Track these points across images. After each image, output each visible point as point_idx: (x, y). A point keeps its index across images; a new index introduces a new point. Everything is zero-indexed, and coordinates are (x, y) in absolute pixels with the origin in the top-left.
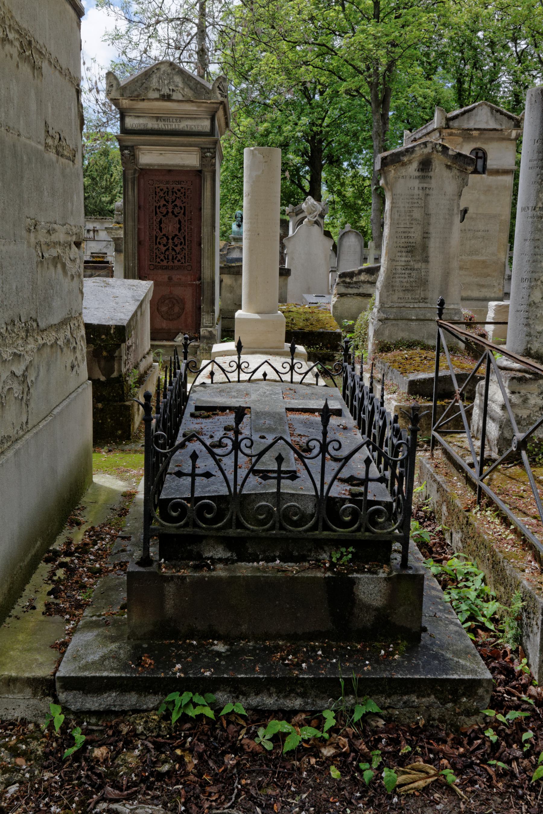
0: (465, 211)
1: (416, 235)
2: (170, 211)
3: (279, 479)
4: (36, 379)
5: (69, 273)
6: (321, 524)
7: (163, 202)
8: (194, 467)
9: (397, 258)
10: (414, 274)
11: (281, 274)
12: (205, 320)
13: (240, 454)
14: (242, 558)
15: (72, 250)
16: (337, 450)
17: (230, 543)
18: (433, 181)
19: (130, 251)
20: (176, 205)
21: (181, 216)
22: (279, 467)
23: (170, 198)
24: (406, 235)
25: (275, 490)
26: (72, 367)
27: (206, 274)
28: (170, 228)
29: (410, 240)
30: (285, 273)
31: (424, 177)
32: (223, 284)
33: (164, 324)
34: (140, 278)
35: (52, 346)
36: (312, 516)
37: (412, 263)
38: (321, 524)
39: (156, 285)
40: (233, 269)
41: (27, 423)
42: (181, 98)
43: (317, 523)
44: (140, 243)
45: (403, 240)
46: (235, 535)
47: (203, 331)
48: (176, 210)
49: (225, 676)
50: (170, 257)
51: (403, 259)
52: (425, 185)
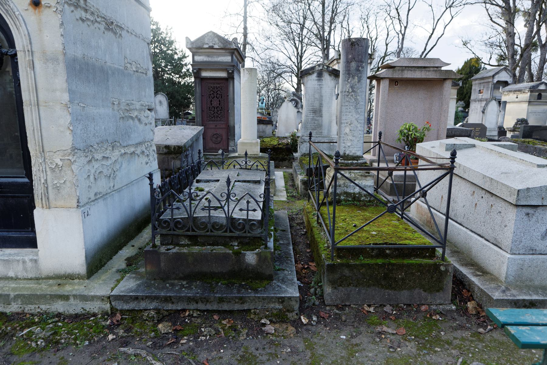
1: (317, 105)
3: (209, 210)
5: (144, 123)
6: (228, 230)
7: (212, 92)
10: (316, 122)
17: (190, 237)
18: (324, 81)
22: (209, 205)
23: (215, 90)
28: (215, 103)
31: (319, 80)
33: (214, 146)
35: (131, 154)
36: (225, 226)
38: (228, 230)
41: (114, 186)
42: (218, 47)
43: (227, 229)
44: (202, 111)
47: (230, 148)
48: (218, 96)
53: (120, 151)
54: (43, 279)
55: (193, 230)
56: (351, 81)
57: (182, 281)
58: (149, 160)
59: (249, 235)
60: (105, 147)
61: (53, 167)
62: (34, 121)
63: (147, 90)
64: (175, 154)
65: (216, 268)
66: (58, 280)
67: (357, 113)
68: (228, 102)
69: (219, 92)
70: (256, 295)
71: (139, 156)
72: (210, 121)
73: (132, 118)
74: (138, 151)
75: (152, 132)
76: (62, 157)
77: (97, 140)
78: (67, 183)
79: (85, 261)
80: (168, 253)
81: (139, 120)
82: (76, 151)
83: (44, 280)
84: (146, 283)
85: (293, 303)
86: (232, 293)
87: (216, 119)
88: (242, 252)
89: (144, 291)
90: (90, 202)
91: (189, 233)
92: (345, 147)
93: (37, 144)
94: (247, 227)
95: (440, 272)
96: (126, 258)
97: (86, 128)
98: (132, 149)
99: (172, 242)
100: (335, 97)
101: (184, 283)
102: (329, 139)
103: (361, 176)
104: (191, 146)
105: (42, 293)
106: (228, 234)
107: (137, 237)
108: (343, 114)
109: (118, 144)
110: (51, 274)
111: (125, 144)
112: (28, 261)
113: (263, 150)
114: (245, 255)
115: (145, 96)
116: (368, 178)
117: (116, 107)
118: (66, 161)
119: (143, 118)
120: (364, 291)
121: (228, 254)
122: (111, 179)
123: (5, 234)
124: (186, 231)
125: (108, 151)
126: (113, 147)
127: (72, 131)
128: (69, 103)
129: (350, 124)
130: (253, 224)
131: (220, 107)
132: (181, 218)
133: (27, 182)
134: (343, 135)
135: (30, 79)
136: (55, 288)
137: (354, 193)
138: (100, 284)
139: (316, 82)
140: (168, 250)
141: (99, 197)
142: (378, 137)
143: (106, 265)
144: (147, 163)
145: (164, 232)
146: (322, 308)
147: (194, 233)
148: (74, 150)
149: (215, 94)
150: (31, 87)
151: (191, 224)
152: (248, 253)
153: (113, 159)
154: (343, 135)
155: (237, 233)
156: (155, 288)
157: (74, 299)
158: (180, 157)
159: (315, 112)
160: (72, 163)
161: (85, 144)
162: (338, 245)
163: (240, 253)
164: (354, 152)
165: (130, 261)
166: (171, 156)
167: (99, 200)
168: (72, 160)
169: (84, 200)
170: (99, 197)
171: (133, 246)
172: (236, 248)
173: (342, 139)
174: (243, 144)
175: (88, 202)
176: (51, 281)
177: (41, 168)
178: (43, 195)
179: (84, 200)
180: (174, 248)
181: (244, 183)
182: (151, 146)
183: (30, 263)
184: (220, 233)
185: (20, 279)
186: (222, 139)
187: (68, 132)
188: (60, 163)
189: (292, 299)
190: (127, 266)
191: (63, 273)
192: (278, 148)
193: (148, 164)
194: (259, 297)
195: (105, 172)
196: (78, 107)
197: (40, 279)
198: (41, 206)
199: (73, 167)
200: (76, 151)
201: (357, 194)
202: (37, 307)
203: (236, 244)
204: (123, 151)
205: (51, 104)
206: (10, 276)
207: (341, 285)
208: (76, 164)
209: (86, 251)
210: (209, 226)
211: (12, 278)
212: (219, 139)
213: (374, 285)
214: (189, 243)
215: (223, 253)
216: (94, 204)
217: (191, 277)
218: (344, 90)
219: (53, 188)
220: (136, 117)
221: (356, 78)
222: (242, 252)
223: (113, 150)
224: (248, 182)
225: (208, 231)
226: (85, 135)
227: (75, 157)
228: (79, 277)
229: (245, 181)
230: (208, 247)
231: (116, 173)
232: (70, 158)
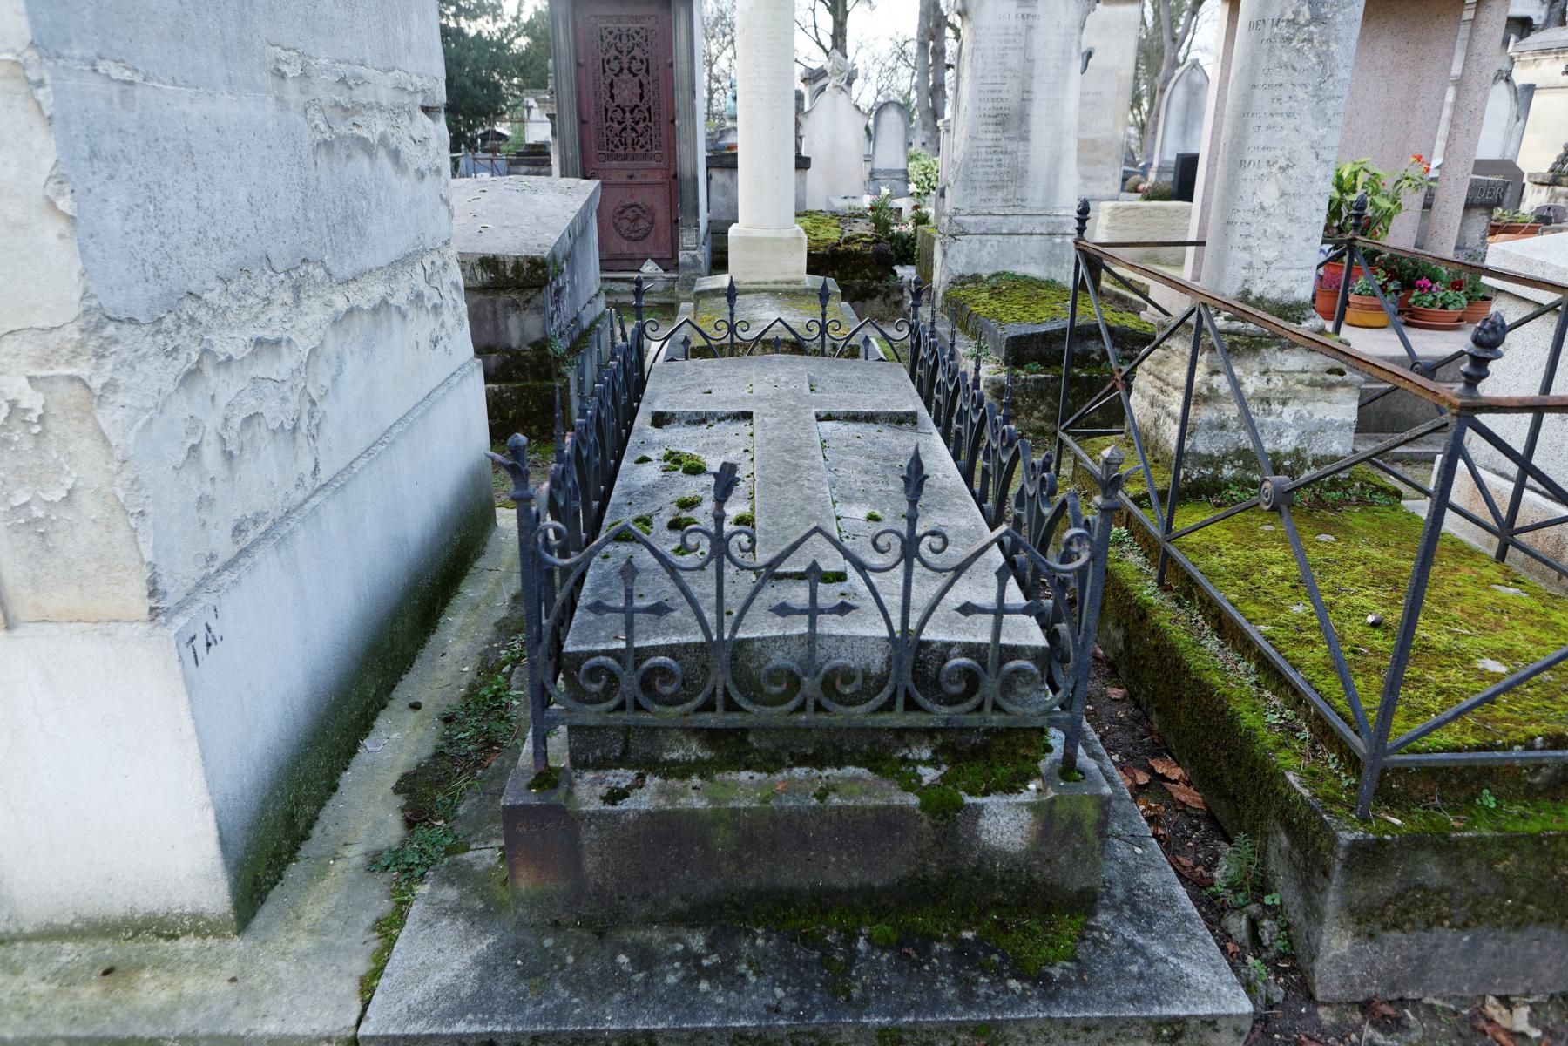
0: (1089, 55)
2: (625, 65)
4: (334, 380)
5: (412, 168)
6: (900, 700)
7: (613, 52)
8: (629, 597)
9: (981, 135)
10: (1006, 160)
11: (798, 167)
12: (686, 239)
13: (730, 571)
14: (739, 760)
15: (417, 122)
16: (937, 552)
17: (711, 736)
19: (568, 133)
20: (634, 58)
21: (642, 74)
23: (625, 44)
24: (995, 95)
25: (806, 630)
26: (435, 342)
27: (684, 167)
29: (1002, 104)
30: (802, 163)
32: (713, 183)
33: (625, 247)
34: (585, 177)
35: (375, 310)
37: (1003, 142)
39: (603, 185)
40: (724, 160)
41: (316, 469)
44: (582, 122)
45: (991, 105)
46: (721, 725)
48: (635, 65)
49: (709, 1025)
50: (629, 142)
51: (990, 136)
52: (1027, 11)
53: (328, 304)
54: (29, 938)
55: (731, 706)
57: (683, 932)
58: (442, 326)
59: (996, 720)
60: (261, 291)
63: (415, 18)
64: (520, 288)
65: (842, 871)
66: (101, 943)
67: (1322, 117)
68: (671, 91)
69: (637, 52)
70: (1057, 1014)
71: (404, 316)
72: (608, 158)
73: (364, 144)
74: (400, 299)
75: (443, 209)
77: (220, 262)
78: (89, 505)
79: (219, 862)
80: (615, 817)
81: (395, 155)
82: (111, 329)
83: (37, 946)
84: (518, 947)
86: (936, 1004)
88: (968, 800)
89: (517, 1005)
90: (219, 571)
91: (712, 720)
92: (1250, 266)
96: (394, 778)
97: (152, 200)
98: (377, 290)
99: (625, 752)
100: (1077, 65)
101: (698, 942)
102: (1049, 224)
103: (1312, 384)
104: (570, 257)
105: (29, 1030)
106: (899, 718)
107: (426, 653)
108: (1254, 122)
109: (319, 273)
111: (347, 272)
113: (817, 263)
114: (977, 811)
115: (409, 49)
116: (1340, 393)
117: (292, 92)
118: (62, 391)
119: (408, 149)
120: (1491, 945)
121: (903, 810)
122: (301, 440)
125: (276, 312)
126: (297, 288)
127: (72, 220)
128: (32, 56)
131: (644, 107)
132: (670, 650)
134: (1249, 217)
136: (90, 993)
138: (302, 957)
140: (614, 796)
141: (258, 535)
143: (316, 832)
144: (435, 342)
145: (591, 715)
146: (1300, 1016)
147: (735, 719)
148: (99, 326)
149: (625, 60)
151: (720, 679)
152: (993, 801)
153: (304, 345)
154: (1249, 217)
156: (567, 984)
158: (539, 300)
159: (1002, 124)
160: (97, 398)
161: (156, 289)
163: (960, 806)
164: (1285, 285)
165: (421, 795)
166: (504, 297)
167: (258, 555)
168: (96, 384)
169: (180, 576)
170: (258, 535)
171: (416, 706)
172: (929, 775)
173: (1239, 230)
174: (748, 242)
175: (207, 577)
176: (69, 952)
179: (180, 576)
180: (640, 782)
181: (855, 428)
182: (445, 266)
186: (652, 223)
187: (51, 231)
188: (32, 400)
189: (1221, 1024)
190: (410, 824)
192: (848, 254)
193: (440, 345)
194: (1068, 1023)
195: (275, 412)
196: (95, 83)
197: (13, 940)
199: (109, 417)
200: (111, 329)
201: (1288, 456)
203: (926, 754)
204: (340, 304)
207: (1395, 926)
208: (121, 398)
209: (218, 814)
210: (810, 685)
212: (643, 224)
213: (1542, 920)
214: (707, 755)
215: (877, 809)
216: (235, 583)
217: (725, 915)
218: (1274, 13)
220: (383, 140)
222: (968, 800)
223: (297, 300)
224: (870, 418)
225: (801, 708)
226: (153, 239)
227: (108, 364)
228: (200, 926)
229: (854, 418)
230: (799, 772)
231: (322, 406)
232: (83, 369)
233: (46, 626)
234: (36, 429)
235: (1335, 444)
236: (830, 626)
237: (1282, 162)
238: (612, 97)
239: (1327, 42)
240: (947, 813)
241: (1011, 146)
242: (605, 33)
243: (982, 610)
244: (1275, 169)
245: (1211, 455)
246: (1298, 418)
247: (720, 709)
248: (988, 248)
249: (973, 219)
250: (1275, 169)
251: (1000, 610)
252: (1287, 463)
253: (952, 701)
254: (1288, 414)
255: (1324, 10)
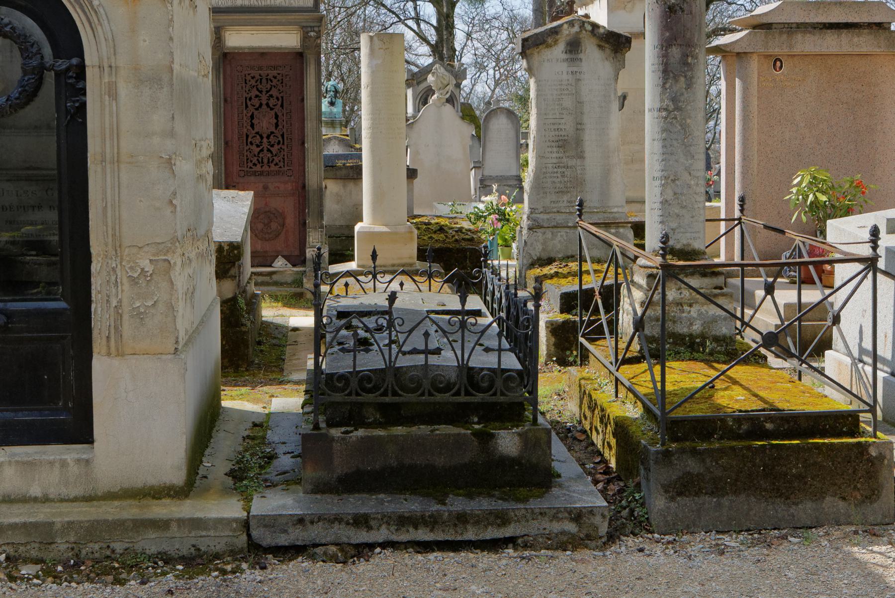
0: (624, 97)
2: (264, 102)
7: (255, 92)
9: (548, 155)
10: (568, 173)
18: (584, 64)
20: (271, 96)
21: (278, 109)
23: (264, 86)
24: (556, 127)
29: (563, 133)
31: (572, 60)
36: (455, 384)
37: (565, 160)
43: (459, 389)
45: (553, 133)
48: (272, 102)
50: (265, 161)
51: (554, 155)
52: (575, 69)
55: (395, 394)
56: (671, 87)
61: (136, 275)
62: (109, 191)
69: (274, 92)
76: (154, 255)
85: (597, 520)
87: (266, 168)
93: (110, 232)
94: (499, 383)
95: (871, 460)
100: (615, 105)
106: (462, 399)
110: (117, 489)
112: (72, 464)
113: (422, 255)
123: (9, 415)
124: (381, 395)
129: (673, 181)
130: (509, 378)
133: (65, 309)
135: (107, 116)
137: (691, 336)
139: (565, 64)
142: (737, 208)
147: (396, 399)
150: (107, 131)
155: (479, 397)
157: (179, 527)
162: (673, 415)
177: (113, 278)
178: (113, 331)
180: (356, 430)
183: (75, 468)
184: (446, 397)
185: (52, 501)
186: (283, 225)
188: (149, 268)
191: (139, 484)
198: (104, 351)
202: (105, 546)
203: (476, 420)
205: (141, 158)
206: (33, 495)
211: (35, 500)
219: (132, 317)
221: (682, 79)
225: (423, 394)
233: (135, 356)
234: (149, 278)
235: (724, 329)
236: (433, 360)
237: (672, 177)
238: (252, 126)
239: (684, 119)
240: (485, 438)
241: (571, 163)
242: (249, 78)
243: (493, 350)
244: (669, 181)
245: (654, 337)
246: (700, 314)
247: (390, 395)
248: (559, 238)
249: (546, 216)
250: (669, 181)
251: (500, 350)
252: (698, 340)
253: (484, 391)
254: (694, 312)
255: (680, 104)
